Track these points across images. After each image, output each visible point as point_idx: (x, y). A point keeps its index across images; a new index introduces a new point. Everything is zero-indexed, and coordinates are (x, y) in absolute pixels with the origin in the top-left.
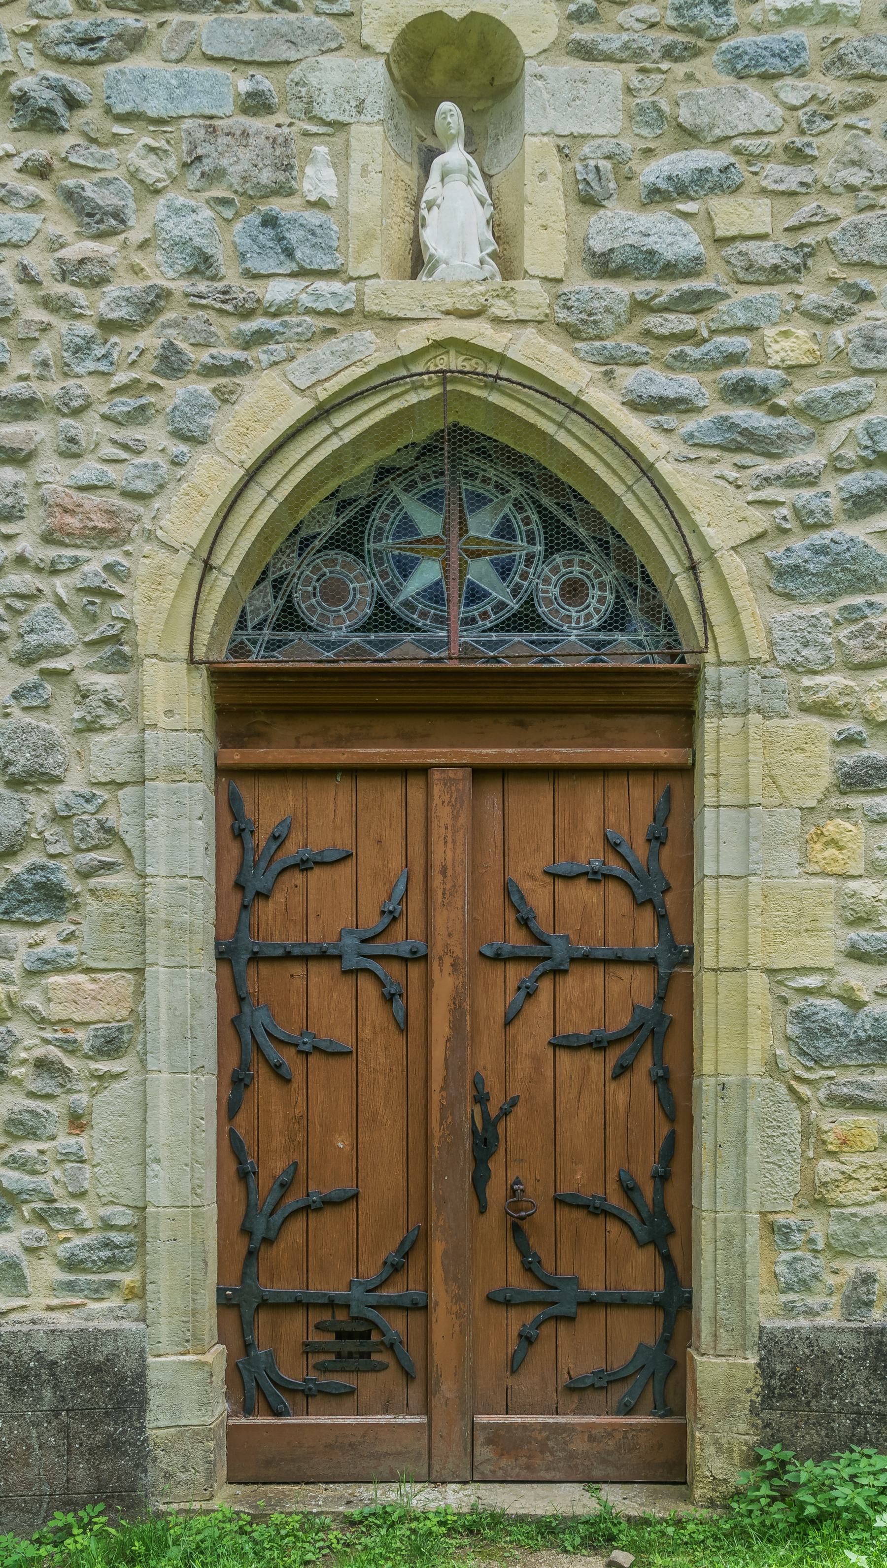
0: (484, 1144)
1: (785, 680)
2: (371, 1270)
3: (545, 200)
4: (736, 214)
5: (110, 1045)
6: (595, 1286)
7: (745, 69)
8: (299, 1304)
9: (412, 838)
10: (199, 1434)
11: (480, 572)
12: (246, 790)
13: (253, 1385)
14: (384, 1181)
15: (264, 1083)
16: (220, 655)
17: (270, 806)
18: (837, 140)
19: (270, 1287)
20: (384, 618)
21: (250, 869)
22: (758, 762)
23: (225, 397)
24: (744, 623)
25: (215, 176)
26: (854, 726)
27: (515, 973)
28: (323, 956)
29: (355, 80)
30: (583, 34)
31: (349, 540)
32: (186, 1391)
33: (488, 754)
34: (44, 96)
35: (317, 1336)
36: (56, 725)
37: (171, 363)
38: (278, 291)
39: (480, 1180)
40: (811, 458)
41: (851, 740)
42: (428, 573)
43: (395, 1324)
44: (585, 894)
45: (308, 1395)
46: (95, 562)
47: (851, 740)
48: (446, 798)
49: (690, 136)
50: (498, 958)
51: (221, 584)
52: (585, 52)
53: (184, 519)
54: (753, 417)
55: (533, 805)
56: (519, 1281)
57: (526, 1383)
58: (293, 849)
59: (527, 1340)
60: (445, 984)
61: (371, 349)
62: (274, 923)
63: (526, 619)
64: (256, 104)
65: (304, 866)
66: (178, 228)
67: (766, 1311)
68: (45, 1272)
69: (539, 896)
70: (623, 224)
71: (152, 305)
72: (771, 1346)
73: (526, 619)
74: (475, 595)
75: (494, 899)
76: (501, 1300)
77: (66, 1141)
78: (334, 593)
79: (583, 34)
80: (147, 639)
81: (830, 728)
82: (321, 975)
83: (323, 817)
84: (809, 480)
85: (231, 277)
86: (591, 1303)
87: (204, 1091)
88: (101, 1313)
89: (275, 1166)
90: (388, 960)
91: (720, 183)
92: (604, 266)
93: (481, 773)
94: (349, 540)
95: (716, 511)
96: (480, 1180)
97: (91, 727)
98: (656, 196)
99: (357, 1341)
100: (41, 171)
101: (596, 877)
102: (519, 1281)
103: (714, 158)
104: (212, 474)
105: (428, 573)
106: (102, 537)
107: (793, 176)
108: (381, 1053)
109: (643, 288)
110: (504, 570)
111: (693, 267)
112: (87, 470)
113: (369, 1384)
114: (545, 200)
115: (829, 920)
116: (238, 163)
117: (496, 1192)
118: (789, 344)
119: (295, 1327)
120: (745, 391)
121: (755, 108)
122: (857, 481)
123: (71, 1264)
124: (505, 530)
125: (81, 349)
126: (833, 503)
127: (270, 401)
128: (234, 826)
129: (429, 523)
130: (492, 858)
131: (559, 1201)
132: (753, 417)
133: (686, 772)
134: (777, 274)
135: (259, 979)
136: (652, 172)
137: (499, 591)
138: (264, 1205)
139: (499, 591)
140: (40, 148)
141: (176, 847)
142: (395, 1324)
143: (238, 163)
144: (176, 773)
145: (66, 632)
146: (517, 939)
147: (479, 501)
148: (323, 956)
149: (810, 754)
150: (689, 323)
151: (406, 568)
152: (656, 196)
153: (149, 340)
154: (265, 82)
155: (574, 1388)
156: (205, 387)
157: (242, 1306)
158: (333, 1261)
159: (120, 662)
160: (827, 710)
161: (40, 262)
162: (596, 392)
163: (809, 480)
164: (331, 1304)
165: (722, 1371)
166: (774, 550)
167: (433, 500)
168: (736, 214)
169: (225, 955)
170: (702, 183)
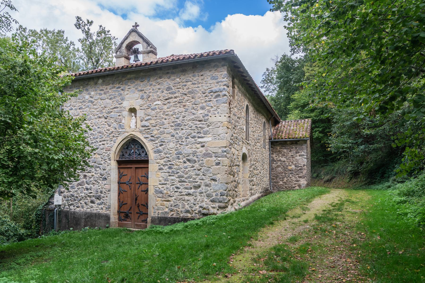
0: (136, 199)
1: (155, 161)
2: (128, 210)
3: (139, 121)
4: (152, 122)
5: (109, 191)
6: (144, 212)
7: (152, 109)
8: (123, 212)
9: (129, 173)
10: (115, 222)
11: (136, 151)
12: (120, 169)
13: (120, 219)
14: (129, 202)
15: (121, 194)
16: (118, 159)
17: (122, 171)
18: (159, 115)
19: (121, 211)
20: (130, 155)
21: (120, 176)
22: (153, 167)
23: (117, 139)
24: (152, 156)
25: (117, 122)
26: (160, 164)
27: (139, 185)
28: (125, 183)
29: (126, 113)
30: (141, 108)
31: (127, 148)
32: (114, 218)
33: (136, 166)
34: (106, 117)
35: (124, 215)
36: (106, 165)
37: (114, 137)
38: (120, 130)
39: (136, 202)
40: (157, 142)
41: (159, 166)
42: (133, 151)
43: (130, 215)
44: (143, 178)
45: (124, 220)
46: (109, 152)
47: (159, 166)
48: (133, 170)
49: (149, 115)
50: (137, 184)
51: (116, 154)
52: (141, 109)
53: (114, 149)
54: (153, 138)
55: (140, 170)
56: (139, 212)
57: (140, 220)
58: (123, 174)
59: (139, 217)
60: (133, 186)
61: (127, 134)
62: (122, 181)
63: (140, 154)
64: (119, 116)
65: (124, 176)
66: (114, 126)
67: (152, 215)
68: (104, 209)
69: (140, 178)
70: (144, 123)
71: (112, 132)
72: (152, 217)
73: (140, 154)
74: (136, 152)
75: (137, 179)
76: (137, 213)
77: (106, 198)
78: (126, 153)
79: (141, 108)
80: (111, 159)
81: (158, 165)
82: (125, 185)
83: (125, 172)
84: (157, 144)
85: (118, 130)
86: (144, 214)
87: (116, 194)
88: (108, 212)
89: (121, 201)
90: (129, 184)
91: (149, 119)
92: (142, 127)
93: (136, 168)
94: (127, 148)
95: (149, 146)
96: (136, 202)
97: (108, 165)
98: (146, 121)
99: (127, 216)
100: (106, 122)
101: (144, 177)
102: (139, 212)
103: (150, 117)
104: (116, 145)
105: (133, 151)
106: (109, 150)
107: (156, 118)
108: (129, 191)
109: (146, 128)
110: (138, 150)
111: (148, 126)
112: (108, 145)
113: (128, 219)
114: (139, 121)
115: (158, 181)
116: (118, 120)
117: (137, 204)
118: (155, 132)
119: (123, 214)
120: (152, 136)
121: (153, 112)
122: (160, 143)
123: (106, 208)
124: (138, 147)
125: (108, 136)
126: (159, 146)
127: (120, 139)
128: (119, 172)
129: (133, 147)
130: (137, 175)
131: (142, 205)
132: (153, 138)
133: (148, 167)
134: (154, 126)
135: (121, 185)
136: (146, 119)
137: (138, 152)
138: (121, 204)
139: (138, 152)
140: (106, 120)
141: (114, 175)
142: (130, 215)
143: (118, 120)
144: (113, 169)
145: (107, 158)
146: (139, 182)
147: (136, 145)
148: (125, 183)
149: (157, 167)
150: (148, 131)
151: (131, 150)
152: (146, 121)
153: (112, 135)
154: (120, 114)
155: (142, 221)
156: (116, 138)
157: (119, 212)
158: (125, 209)
159: (110, 160)
160: (158, 163)
161: (105, 129)
162: (141, 137)
163: (157, 144)
164: (125, 213)
165: (149, 219)
166: (154, 150)
167: (133, 145)
168: (152, 122)
169: (118, 183)
170: (149, 119)
